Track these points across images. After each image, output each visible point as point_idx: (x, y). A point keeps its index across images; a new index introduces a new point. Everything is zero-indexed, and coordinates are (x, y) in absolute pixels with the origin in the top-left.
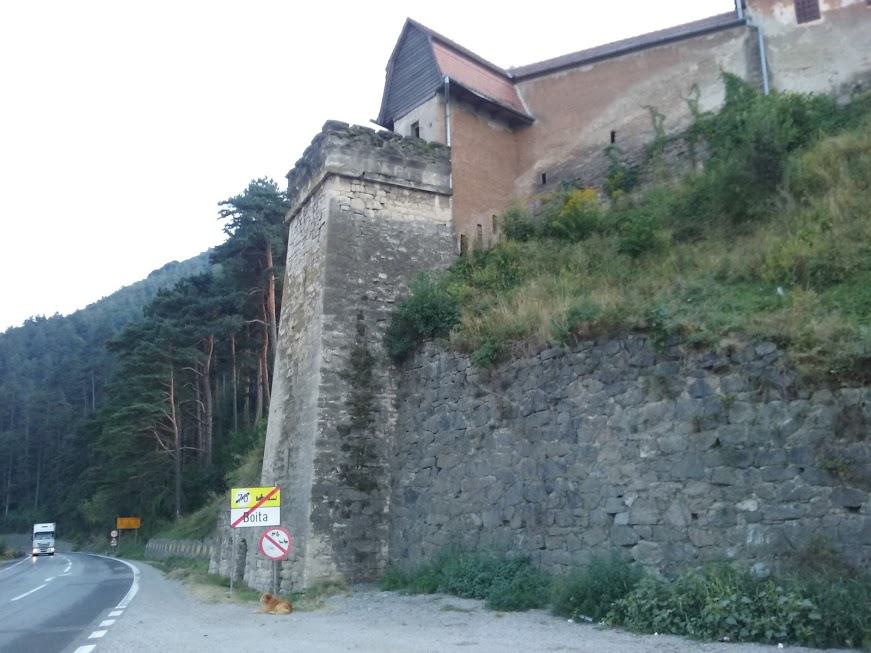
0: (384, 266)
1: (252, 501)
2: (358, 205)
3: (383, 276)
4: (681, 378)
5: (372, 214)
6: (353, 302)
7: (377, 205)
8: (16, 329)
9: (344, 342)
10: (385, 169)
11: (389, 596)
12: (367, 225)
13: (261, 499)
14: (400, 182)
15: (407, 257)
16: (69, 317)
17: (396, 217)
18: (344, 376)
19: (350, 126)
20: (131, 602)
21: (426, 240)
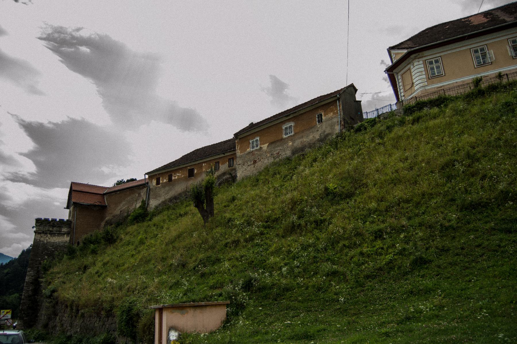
0: (47, 254)
1: (5, 313)
2: (42, 239)
3: (46, 257)
4: (297, 206)
5: (45, 241)
6: (36, 264)
7: (47, 239)
8: (15, 259)
9: (33, 275)
10: (51, 229)
11: (200, 218)
12: (44, 244)
13: (7, 313)
14: (54, 232)
15: (53, 251)
16: (20, 256)
17: (52, 241)
18: (31, 283)
19: (58, 220)
20: (206, 194)
21: (60, 247)
